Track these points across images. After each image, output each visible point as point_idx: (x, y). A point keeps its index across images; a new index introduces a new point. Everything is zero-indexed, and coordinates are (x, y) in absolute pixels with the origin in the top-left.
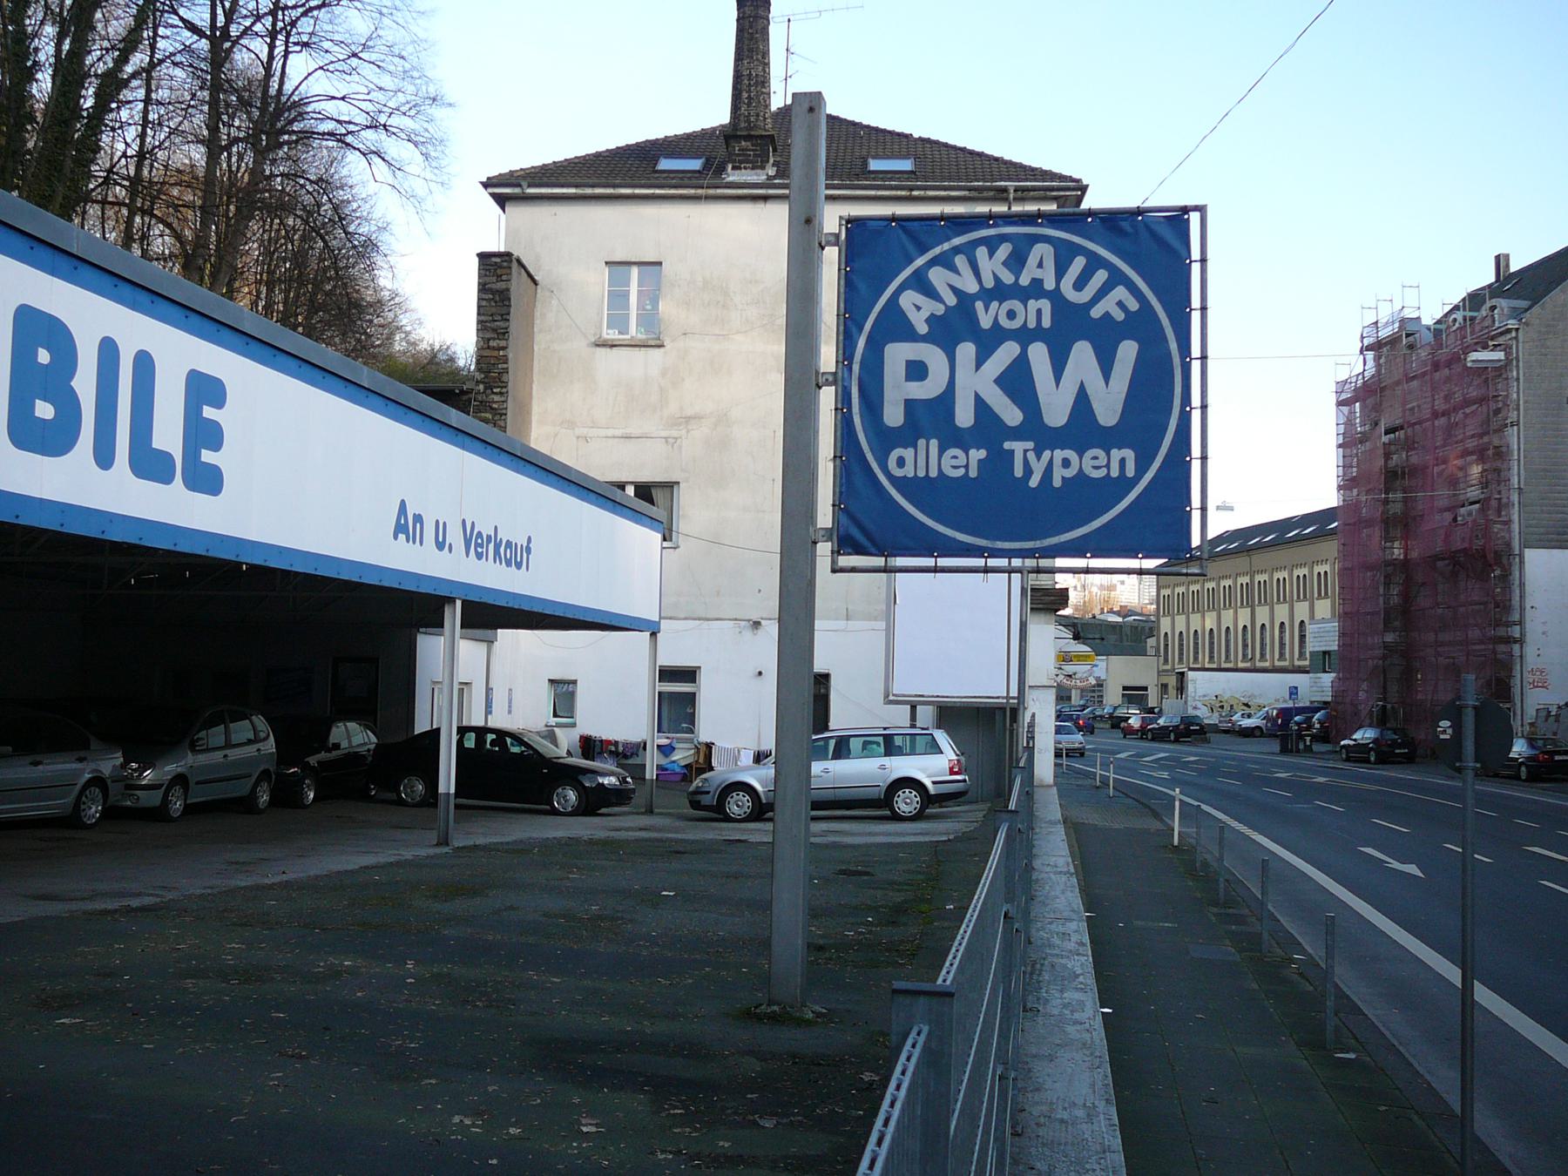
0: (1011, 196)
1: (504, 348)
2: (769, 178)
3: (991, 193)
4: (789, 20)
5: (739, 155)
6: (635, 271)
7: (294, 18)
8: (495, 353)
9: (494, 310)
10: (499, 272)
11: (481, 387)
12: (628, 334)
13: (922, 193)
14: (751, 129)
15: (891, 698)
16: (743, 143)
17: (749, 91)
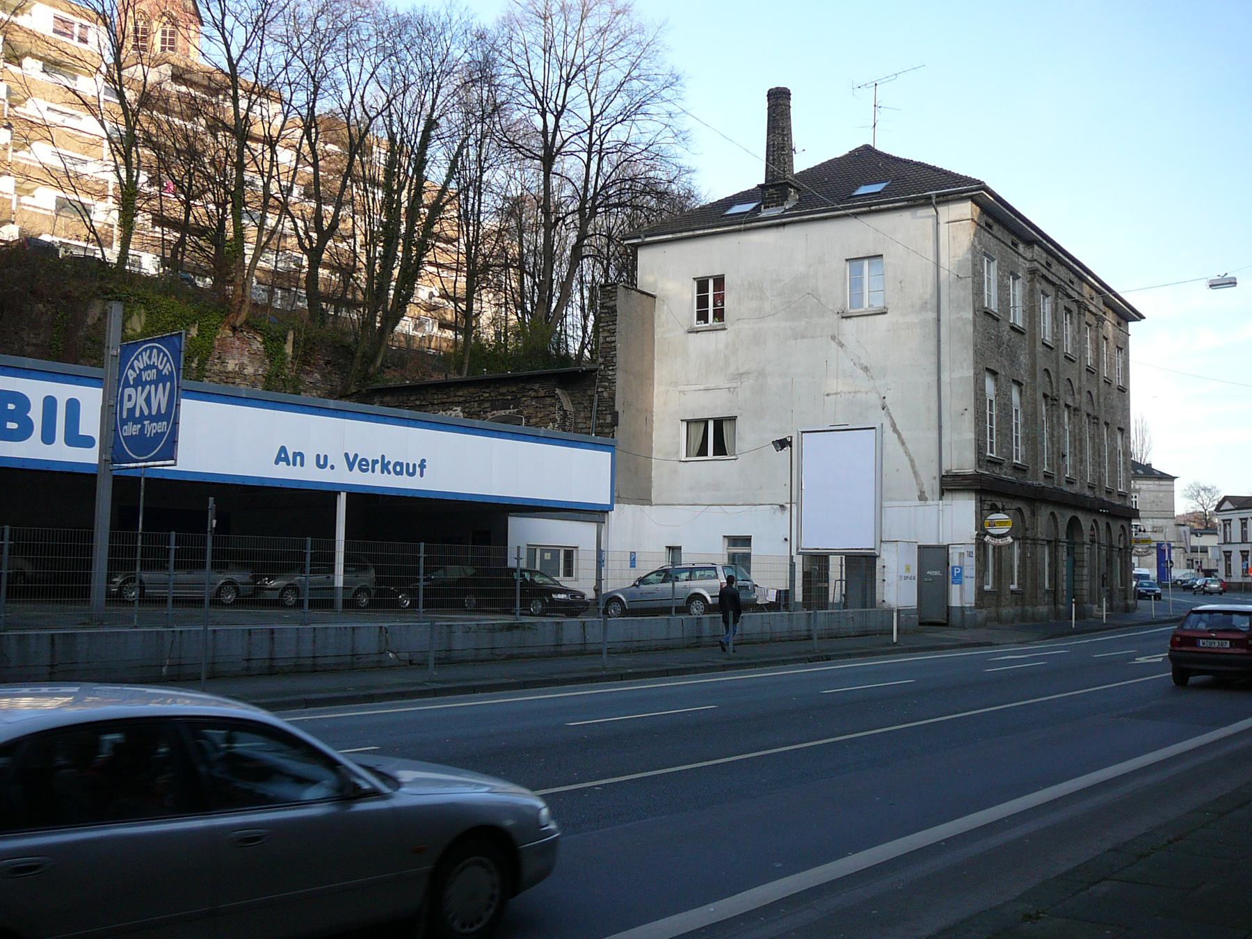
0: (934, 201)
1: (614, 342)
2: (786, 210)
3: (922, 201)
4: (876, 85)
5: (768, 198)
6: (866, 262)
7: (541, 153)
8: (609, 345)
9: (608, 319)
10: (611, 295)
11: (602, 367)
12: (862, 307)
13: (877, 207)
14: (775, 180)
15: (800, 551)
16: (771, 190)
17: (774, 155)
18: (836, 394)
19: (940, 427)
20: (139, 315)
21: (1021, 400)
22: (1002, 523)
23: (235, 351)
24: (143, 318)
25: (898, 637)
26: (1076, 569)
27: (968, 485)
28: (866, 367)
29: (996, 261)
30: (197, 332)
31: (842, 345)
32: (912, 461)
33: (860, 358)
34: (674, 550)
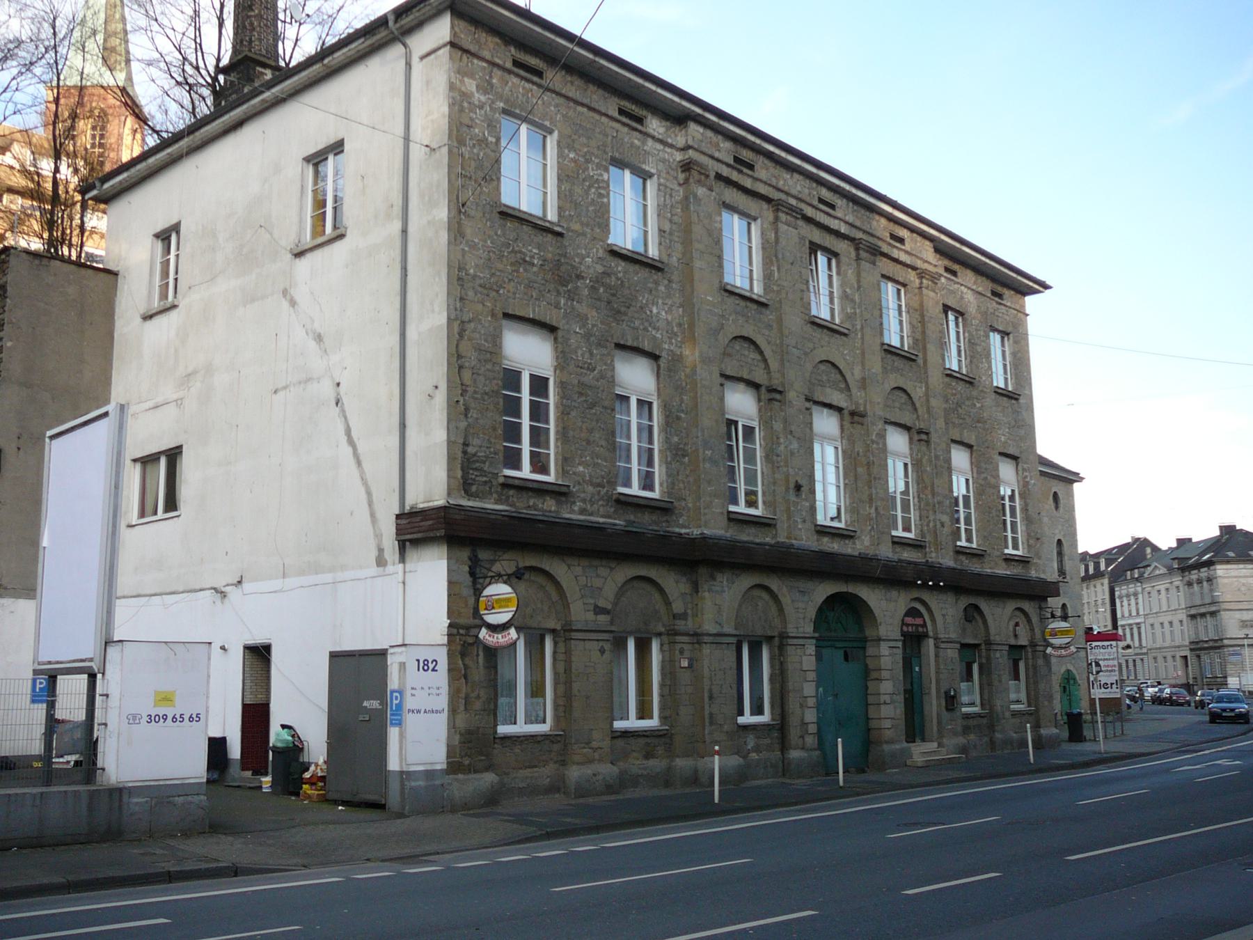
18: (285, 388)
19: (403, 426)
21: (658, 384)
22: (503, 602)
26: (869, 684)
27: (430, 529)
29: (556, 134)
31: (293, 303)
32: (369, 494)
33: (313, 321)
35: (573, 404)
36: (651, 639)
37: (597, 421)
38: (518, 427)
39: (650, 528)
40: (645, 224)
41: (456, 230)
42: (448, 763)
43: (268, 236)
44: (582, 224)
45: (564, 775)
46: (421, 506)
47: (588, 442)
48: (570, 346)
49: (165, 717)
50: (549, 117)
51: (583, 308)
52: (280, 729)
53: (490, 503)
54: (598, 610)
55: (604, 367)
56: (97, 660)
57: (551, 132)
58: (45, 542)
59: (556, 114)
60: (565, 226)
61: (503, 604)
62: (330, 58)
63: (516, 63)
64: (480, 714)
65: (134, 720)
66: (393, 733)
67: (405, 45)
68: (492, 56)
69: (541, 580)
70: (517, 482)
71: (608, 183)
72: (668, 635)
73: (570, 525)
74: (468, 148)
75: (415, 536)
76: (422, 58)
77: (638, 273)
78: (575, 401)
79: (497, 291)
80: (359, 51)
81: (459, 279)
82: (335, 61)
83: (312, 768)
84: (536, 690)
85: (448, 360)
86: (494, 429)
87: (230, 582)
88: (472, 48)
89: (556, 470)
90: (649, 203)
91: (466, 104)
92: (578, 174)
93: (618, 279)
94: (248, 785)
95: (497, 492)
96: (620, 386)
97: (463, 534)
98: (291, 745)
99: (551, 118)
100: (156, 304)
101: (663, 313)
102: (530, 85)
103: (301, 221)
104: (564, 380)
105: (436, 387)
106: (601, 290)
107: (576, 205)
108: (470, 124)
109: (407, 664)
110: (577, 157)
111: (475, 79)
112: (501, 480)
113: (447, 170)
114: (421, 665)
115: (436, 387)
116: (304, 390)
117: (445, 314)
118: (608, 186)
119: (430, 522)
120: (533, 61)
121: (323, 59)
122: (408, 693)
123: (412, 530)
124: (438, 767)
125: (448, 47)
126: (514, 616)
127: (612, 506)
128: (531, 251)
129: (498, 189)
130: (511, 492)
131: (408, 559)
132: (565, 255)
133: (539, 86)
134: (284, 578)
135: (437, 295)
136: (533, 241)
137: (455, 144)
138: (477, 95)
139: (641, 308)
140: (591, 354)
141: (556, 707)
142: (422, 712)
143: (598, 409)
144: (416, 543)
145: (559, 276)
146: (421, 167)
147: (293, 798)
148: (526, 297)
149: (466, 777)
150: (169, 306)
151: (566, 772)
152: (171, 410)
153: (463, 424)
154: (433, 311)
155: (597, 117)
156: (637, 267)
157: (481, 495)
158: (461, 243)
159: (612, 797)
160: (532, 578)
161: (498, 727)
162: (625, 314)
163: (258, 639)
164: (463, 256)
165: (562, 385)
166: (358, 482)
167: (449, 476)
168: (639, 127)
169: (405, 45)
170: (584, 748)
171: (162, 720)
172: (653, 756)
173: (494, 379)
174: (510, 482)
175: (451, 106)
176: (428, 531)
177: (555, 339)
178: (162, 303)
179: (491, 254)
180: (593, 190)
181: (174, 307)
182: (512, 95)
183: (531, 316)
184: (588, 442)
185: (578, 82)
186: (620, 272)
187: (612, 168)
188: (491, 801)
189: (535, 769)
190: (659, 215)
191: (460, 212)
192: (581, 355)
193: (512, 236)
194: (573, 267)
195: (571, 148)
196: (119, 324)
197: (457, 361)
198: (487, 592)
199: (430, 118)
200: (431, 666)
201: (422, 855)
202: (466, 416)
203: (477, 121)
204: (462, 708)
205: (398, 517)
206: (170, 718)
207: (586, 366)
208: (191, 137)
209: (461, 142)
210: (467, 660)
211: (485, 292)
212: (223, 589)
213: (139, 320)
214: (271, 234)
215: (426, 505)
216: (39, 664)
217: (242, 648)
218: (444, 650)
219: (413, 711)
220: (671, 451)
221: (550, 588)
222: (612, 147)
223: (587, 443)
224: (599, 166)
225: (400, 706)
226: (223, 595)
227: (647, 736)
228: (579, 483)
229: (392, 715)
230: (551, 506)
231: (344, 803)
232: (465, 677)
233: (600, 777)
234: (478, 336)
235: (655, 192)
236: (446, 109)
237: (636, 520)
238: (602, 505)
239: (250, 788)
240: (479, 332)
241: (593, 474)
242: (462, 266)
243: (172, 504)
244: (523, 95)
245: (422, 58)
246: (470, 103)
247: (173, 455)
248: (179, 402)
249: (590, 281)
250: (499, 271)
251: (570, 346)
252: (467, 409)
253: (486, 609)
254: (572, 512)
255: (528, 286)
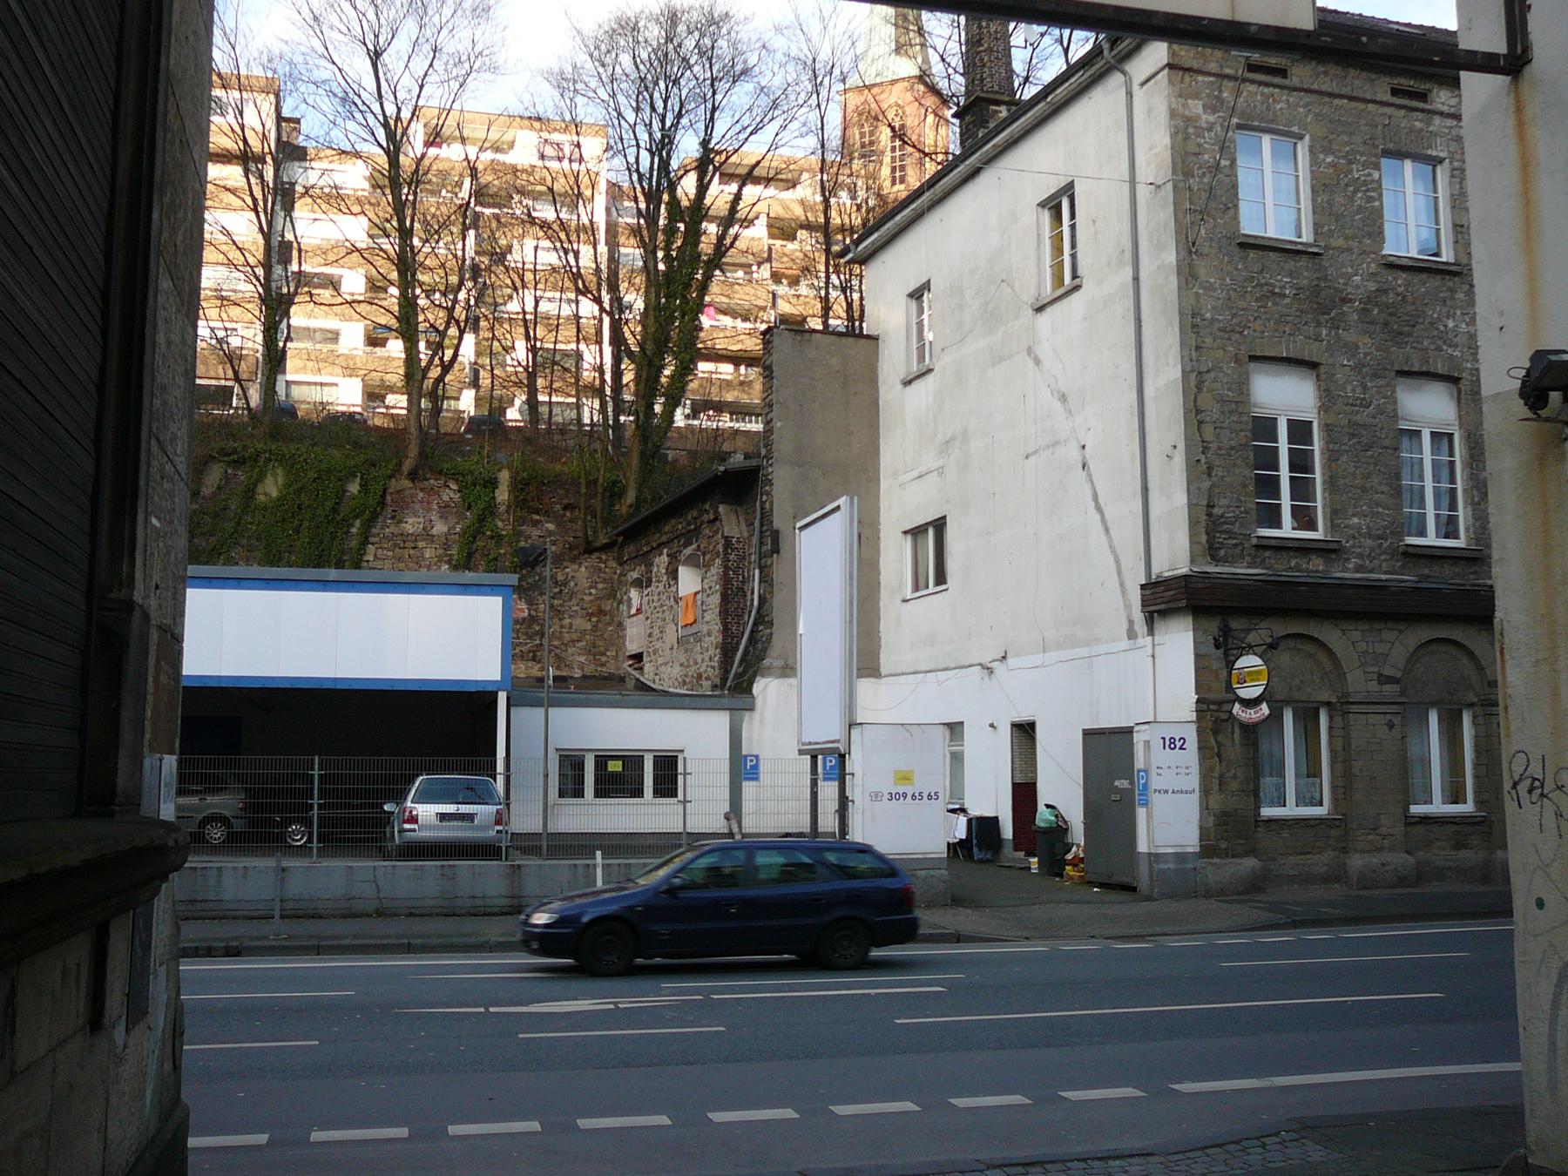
18: (1035, 452)
19: (1145, 489)
20: (275, 476)
21: (1460, 411)
23: (417, 506)
24: (280, 480)
25: (397, 1125)
28: (1063, 395)
29: (1307, 138)
30: (359, 488)
31: (1037, 362)
32: (1117, 562)
34: (690, 774)
35: (1343, 447)
36: (1461, 710)
37: (1376, 464)
38: (1275, 481)
39: (1452, 581)
40: (1437, 223)
41: (1187, 273)
42: (1201, 846)
43: (1010, 290)
44: (1347, 238)
45: (1345, 864)
46: (1166, 574)
47: (1364, 490)
48: (1336, 382)
49: (905, 795)
50: (1296, 122)
51: (1350, 336)
52: (1045, 808)
53: (1242, 568)
54: (1383, 679)
55: (1382, 401)
56: (843, 741)
57: (1301, 138)
58: (801, 630)
59: (1306, 116)
60: (1323, 244)
61: (1254, 677)
62: (1053, 96)
63: (1252, 68)
64: (1237, 795)
65: (876, 797)
66: (1141, 813)
67: (1124, 73)
68: (1221, 67)
69: (1309, 647)
70: (1273, 543)
71: (1379, 182)
72: (1482, 705)
73: (1342, 585)
74: (1197, 179)
75: (1162, 607)
76: (1143, 84)
77: (1425, 283)
78: (1345, 444)
79: (1241, 333)
80: (1080, 84)
81: (1194, 326)
82: (1058, 98)
83: (1074, 849)
84: (1311, 770)
85: (1185, 416)
86: (1245, 486)
87: (996, 657)
88: (1195, 65)
89: (1325, 524)
90: (1440, 195)
91: (1191, 130)
92: (1338, 180)
93: (1398, 294)
94: (1018, 865)
95: (1250, 555)
96: (1402, 419)
97: (1206, 604)
98: (1055, 826)
99: (1300, 121)
100: (915, 368)
101: (1464, 326)
102: (1271, 89)
103: (1040, 273)
104: (1328, 422)
105: (1175, 447)
106: (1376, 311)
107: (1338, 217)
108: (1197, 151)
109: (1151, 743)
110: (1336, 160)
111: (1201, 99)
112: (1254, 541)
113: (1172, 208)
114: (1167, 743)
115: (1175, 447)
116: (1053, 454)
117: (1179, 367)
118: (1381, 185)
119: (1173, 592)
120: (1273, 60)
121: (1046, 97)
122: (1154, 772)
123: (1154, 602)
124: (1191, 850)
125: (1166, 70)
126: (1265, 689)
127: (1397, 561)
128: (1281, 280)
129: (1236, 218)
130: (1267, 554)
131: (1156, 632)
132: (1325, 278)
133: (1282, 87)
134: (1044, 652)
135: (1171, 347)
136: (1282, 268)
137: (1181, 177)
138: (1204, 117)
139: (1432, 324)
140: (1365, 387)
141: (1334, 788)
142: (1170, 792)
143: (1376, 451)
144: (1164, 614)
145: (1317, 303)
146: (1148, 207)
147: (1057, 879)
148: (1276, 334)
149: (1224, 861)
150: (924, 370)
151: (1348, 861)
152: (934, 477)
153: (1208, 484)
154: (1168, 364)
155: (1361, 106)
156: (1424, 276)
157: (1230, 559)
158: (1194, 286)
159: (1403, 891)
160: (1298, 646)
161: (1262, 809)
162: (1410, 334)
163: (1023, 716)
164: (1198, 301)
165: (1327, 428)
166: (1106, 548)
167: (1191, 543)
168: (1421, 105)
169: (1124, 73)
170: (1369, 834)
171: (902, 798)
172: (1465, 847)
173: (1241, 431)
174: (1265, 542)
175: (1173, 136)
176: (1168, 602)
177: (1318, 376)
178: (921, 366)
179: (1231, 292)
180: (1360, 195)
181: (930, 371)
182: (1249, 105)
183: (1285, 355)
184: (1364, 490)
185: (1334, 70)
186: (1400, 286)
187: (1385, 162)
188: (1254, 887)
189: (1309, 856)
190: (1453, 207)
191: (1191, 252)
192: (1352, 390)
193: (1257, 267)
194: (1337, 290)
195: (1328, 151)
196: (882, 390)
197: (1195, 415)
198: (1240, 663)
199: (1153, 152)
200: (1178, 744)
201: (1150, 936)
202: (1209, 475)
203: (1206, 145)
204: (1216, 788)
205: (1143, 587)
206: (909, 797)
207: (1358, 402)
208: (932, 190)
209: (1188, 174)
210: (1220, 738)
211: (1227, 336)
212: (989, 665)
213: (900, 386)
214: (1012, 289)
215: (1170, 573)
216: (803, 744)
217: (1009, 726)
218: (1194, 727)
219: (1160, 792)
220: (1478, 490)
221: (1322, 657)
222: (1384, 138)
223: (1363, 491)
224: (1365, 165)
225: (1145, 786)
226: (990, 671)
227: (1455, 823)
228: (1354, 538)
229: (1140, 795)
230: (1318, 565)
231: (1101, 885)
232: (1219, 755)
233: (1391, 867)
234: (1219, 385)
235: (1447, 181)
236: (1167, 140)
237: (1432, 574)
238: (1385, 560)
239: (1021, 868)
240: (1221, 382)
241: (1371, 524)
242: (1196, 311)
243: (941, 578)
244: (1262, 104)
245: (1143, 84)
246: (1196, 127)
247: (939, 525)
248: (940, 470)
249: (1360, 303)
250: (1242, 309)
251: (1336, 382)
252: (1210, 468)
253: (1238, 683)
254: (1346, 570)
255: (1279, 322)
